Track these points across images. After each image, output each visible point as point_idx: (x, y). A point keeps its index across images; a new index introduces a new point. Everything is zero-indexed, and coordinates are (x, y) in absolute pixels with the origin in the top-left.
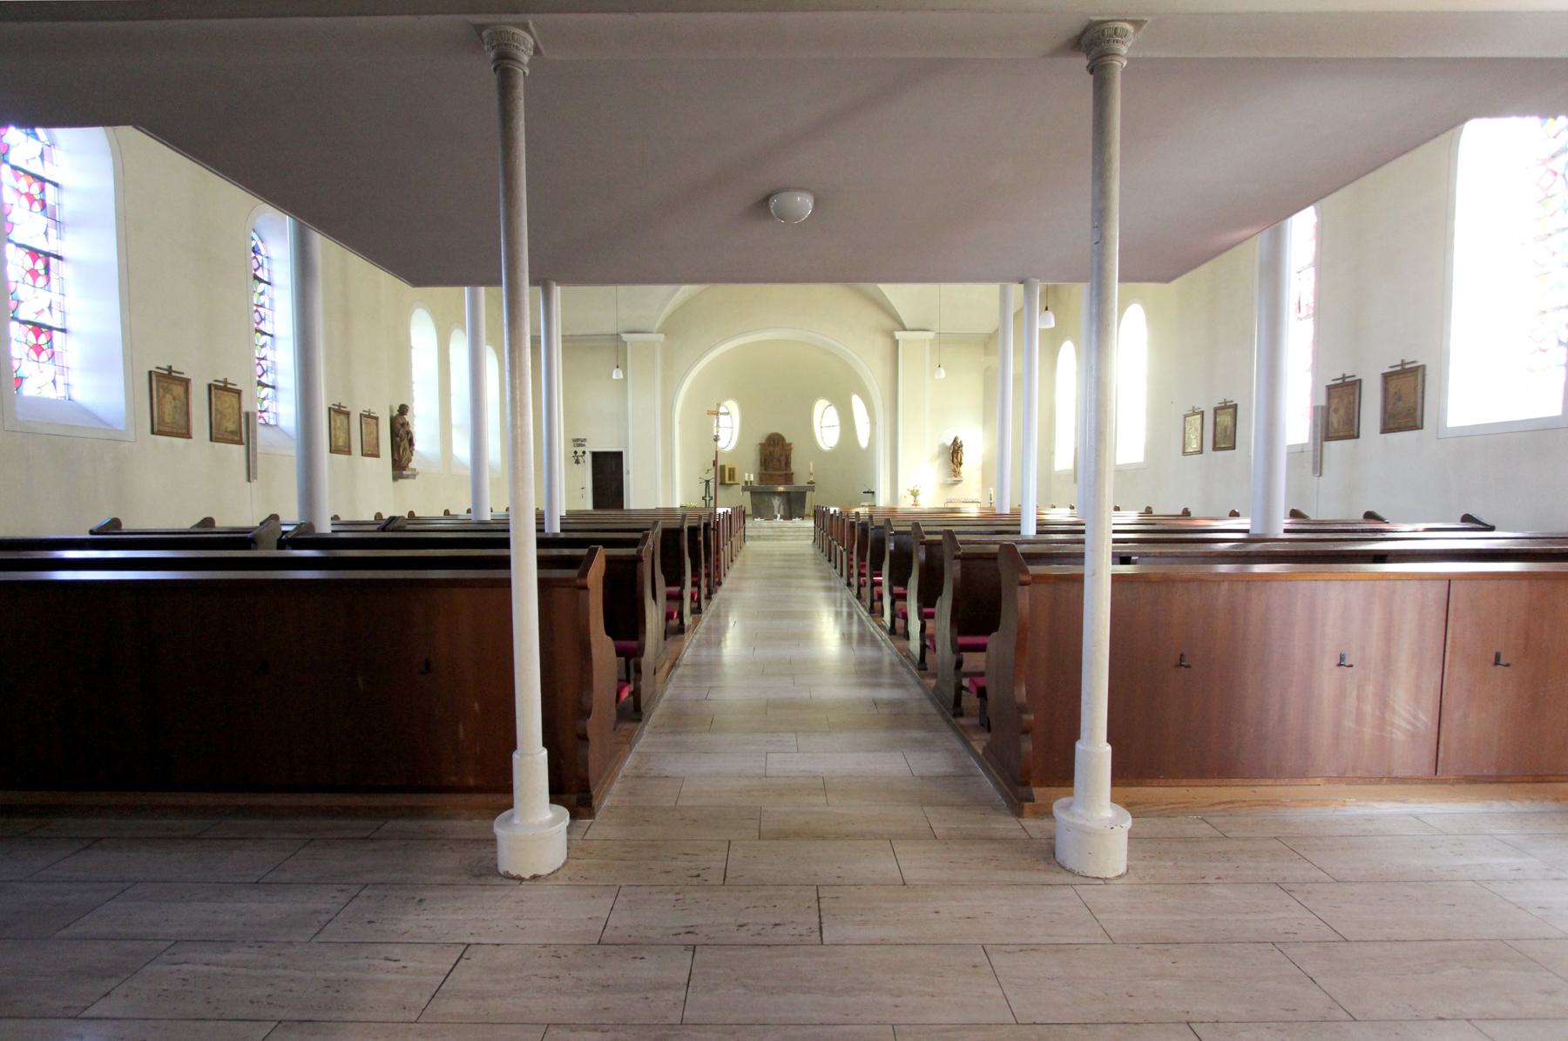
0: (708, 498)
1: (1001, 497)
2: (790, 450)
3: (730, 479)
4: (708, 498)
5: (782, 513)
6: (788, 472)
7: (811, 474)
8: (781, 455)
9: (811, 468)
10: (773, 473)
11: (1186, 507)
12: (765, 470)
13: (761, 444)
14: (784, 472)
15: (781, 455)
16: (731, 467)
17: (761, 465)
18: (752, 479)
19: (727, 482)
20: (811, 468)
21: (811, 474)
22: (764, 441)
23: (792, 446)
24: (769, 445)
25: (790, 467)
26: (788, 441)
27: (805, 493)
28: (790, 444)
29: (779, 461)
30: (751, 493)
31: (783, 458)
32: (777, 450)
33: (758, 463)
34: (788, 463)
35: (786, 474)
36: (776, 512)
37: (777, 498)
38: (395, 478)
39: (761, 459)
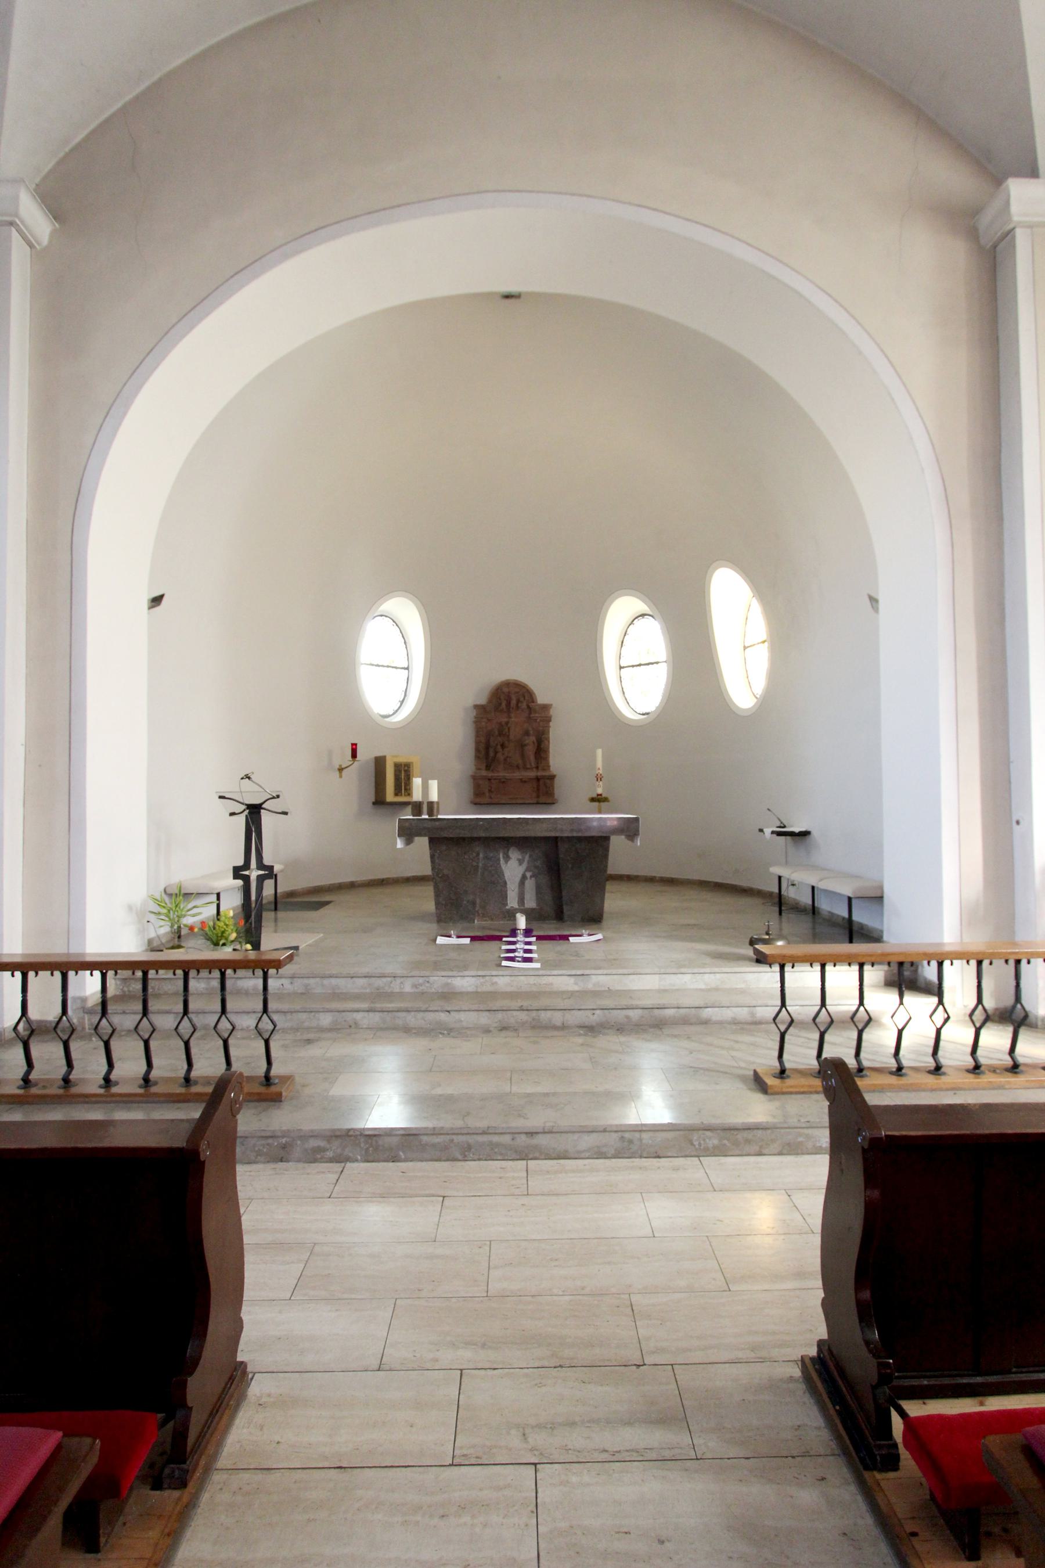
0: (254, 874)
1: (168, 925)
2: (548, 720)
3: (398, 792)
4: (254, 874)
5: (531, 903)
6: (540, 773)
7: (599, 778)
8: (527, 733)
9: (599, 763)
10: (508, 775)
11: (1029, 965)
12: (488, 768)
13: (476, 707)
14: (532, 774)
15: (527, 733)
16: (402, 760)
17: (477, 757)
18: (434, 797)
19: (390, 797)
20: (599, 763)
21: (599, 778)
22: (483, 701)
23: (552, 712)
24: (497, 708)
25: (546, 759)
26: (541, 699)
27: (606, 839)
28: (546, 708)
29: (522, 746)
30: (432, 841)
31: (532, 739)
32: (517, 723)
33: (470, 753)
34: (541, 751)
35: (538, 779)
36: (512, 902)
37: (514, 854)
38: (608, 801)
39: (477, 743)
